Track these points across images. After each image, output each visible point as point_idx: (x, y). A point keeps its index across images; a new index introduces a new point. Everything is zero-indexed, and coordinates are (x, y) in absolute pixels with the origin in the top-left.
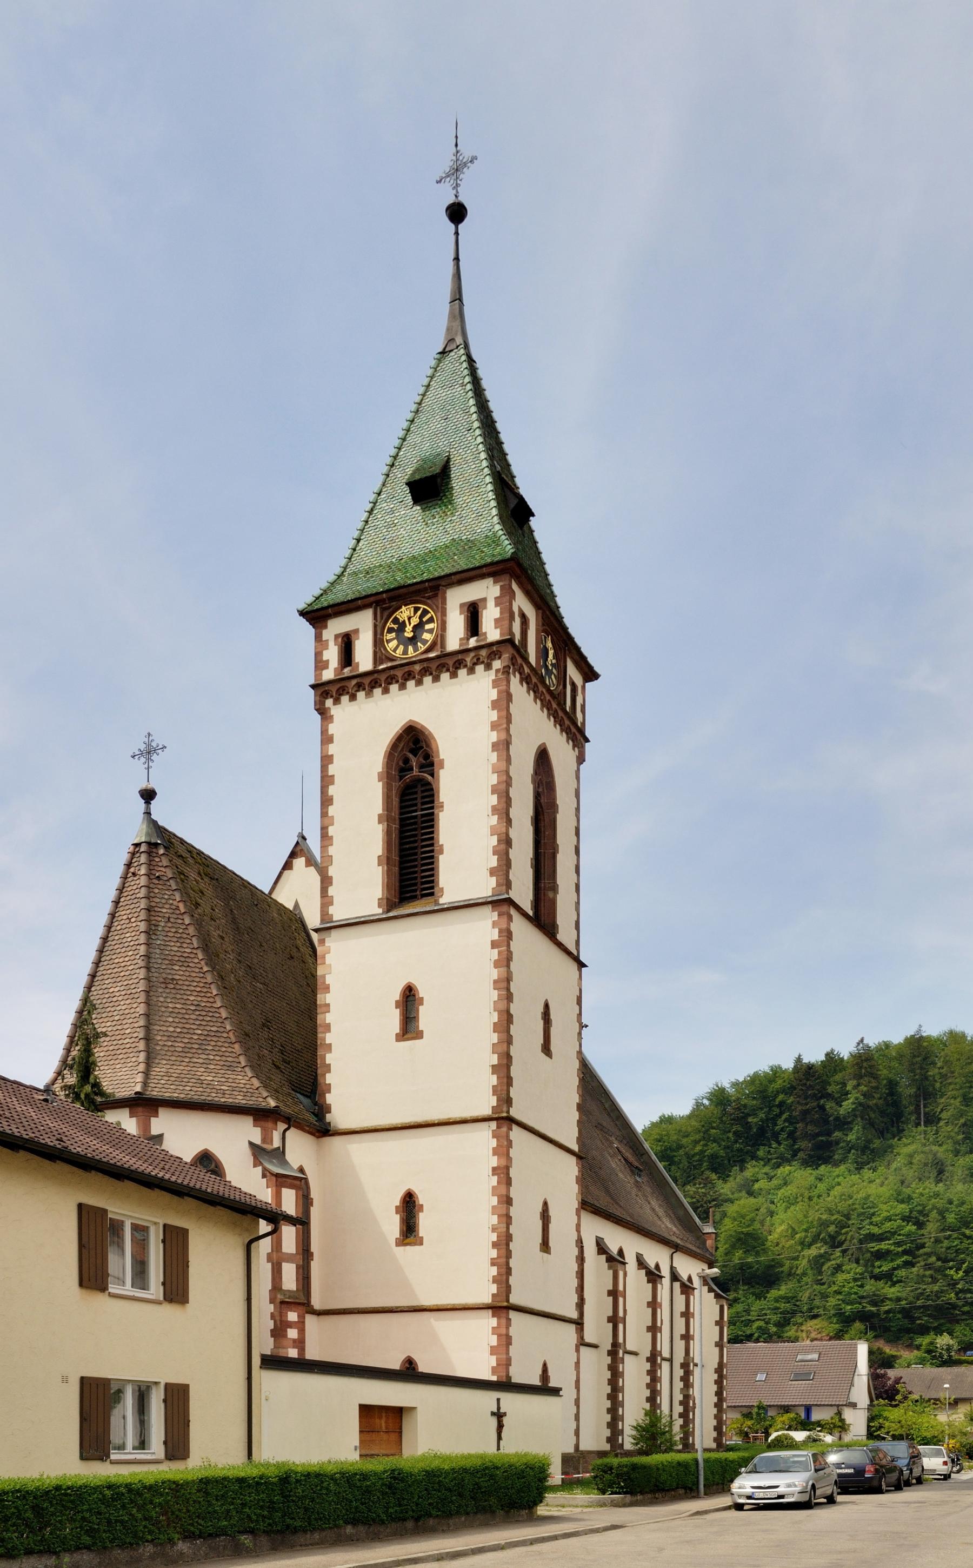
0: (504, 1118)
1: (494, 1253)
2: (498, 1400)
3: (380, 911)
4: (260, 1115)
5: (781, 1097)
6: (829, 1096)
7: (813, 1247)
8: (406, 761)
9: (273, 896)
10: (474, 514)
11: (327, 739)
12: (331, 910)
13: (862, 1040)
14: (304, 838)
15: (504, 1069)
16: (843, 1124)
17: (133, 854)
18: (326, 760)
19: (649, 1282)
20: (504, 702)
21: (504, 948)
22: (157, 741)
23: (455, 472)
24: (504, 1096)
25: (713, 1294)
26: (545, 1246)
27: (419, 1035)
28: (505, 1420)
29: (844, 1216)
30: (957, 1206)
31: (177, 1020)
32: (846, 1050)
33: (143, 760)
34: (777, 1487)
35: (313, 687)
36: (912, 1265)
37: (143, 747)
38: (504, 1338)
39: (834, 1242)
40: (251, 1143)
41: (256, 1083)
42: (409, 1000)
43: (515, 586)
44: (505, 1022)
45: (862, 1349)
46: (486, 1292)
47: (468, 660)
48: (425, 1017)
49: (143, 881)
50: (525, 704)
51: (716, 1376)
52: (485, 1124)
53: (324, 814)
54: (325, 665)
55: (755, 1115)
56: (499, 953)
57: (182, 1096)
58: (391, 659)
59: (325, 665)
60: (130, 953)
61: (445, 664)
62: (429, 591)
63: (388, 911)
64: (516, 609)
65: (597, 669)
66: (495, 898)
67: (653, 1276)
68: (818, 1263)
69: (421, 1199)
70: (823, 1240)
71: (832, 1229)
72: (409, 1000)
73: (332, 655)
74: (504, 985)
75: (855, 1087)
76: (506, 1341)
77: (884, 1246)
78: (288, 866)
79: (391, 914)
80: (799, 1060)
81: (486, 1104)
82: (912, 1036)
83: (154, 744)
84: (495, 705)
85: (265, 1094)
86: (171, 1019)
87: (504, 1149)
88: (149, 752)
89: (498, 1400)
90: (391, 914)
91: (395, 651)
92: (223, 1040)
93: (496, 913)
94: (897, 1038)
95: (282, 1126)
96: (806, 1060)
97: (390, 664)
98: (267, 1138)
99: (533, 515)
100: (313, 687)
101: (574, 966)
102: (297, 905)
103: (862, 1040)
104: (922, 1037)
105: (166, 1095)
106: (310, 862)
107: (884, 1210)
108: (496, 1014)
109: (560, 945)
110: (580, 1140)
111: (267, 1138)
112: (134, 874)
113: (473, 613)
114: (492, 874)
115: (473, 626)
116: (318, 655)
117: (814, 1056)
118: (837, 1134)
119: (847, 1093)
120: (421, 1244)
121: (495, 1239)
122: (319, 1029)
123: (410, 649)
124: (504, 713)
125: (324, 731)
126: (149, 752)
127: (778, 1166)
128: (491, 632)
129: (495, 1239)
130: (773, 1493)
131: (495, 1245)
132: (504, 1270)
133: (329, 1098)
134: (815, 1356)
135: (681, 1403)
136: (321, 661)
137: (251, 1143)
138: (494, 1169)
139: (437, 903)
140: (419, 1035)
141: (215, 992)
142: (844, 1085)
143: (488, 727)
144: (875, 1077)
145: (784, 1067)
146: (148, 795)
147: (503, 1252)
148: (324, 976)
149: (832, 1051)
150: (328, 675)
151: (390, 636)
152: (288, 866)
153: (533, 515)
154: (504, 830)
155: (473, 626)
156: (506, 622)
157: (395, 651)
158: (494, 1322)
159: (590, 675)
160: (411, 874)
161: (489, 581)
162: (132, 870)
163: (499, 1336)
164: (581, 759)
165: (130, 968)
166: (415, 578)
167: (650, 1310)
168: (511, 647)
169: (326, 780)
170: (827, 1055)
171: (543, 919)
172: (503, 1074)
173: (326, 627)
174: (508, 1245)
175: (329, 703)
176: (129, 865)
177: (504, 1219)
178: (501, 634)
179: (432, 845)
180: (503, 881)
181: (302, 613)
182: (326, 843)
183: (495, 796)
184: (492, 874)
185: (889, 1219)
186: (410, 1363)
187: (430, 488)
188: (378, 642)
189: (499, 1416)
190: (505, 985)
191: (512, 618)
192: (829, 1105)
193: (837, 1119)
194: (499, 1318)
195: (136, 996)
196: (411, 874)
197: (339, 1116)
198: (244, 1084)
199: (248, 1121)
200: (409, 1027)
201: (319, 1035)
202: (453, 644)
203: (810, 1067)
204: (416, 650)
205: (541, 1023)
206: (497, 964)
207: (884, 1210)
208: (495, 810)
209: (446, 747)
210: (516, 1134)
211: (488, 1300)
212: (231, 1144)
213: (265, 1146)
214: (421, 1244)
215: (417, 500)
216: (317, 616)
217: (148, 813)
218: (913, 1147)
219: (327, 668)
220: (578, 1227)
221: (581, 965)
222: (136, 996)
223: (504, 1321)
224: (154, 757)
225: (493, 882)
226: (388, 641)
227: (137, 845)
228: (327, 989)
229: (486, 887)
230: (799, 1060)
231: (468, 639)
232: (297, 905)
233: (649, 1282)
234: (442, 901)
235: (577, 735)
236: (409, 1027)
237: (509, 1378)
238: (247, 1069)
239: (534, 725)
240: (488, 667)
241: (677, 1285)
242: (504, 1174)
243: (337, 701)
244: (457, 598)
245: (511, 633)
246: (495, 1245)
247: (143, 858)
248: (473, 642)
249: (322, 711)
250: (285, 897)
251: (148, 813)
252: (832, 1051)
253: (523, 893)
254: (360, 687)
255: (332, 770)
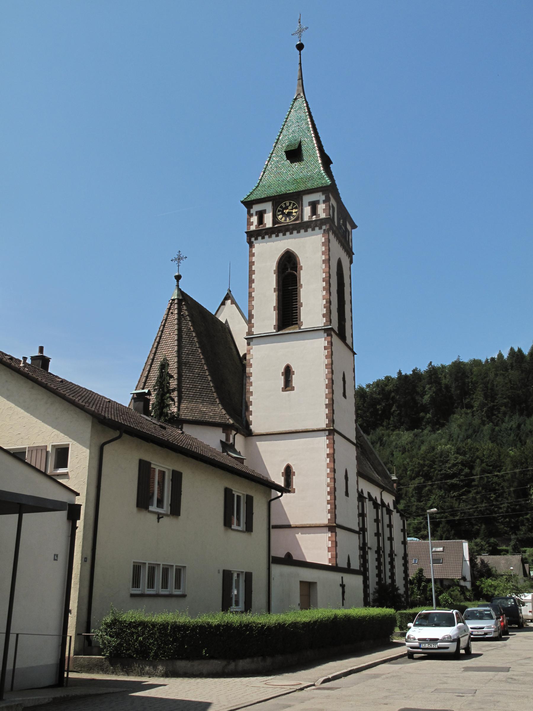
0: (331, 431)
1: (329, 498)
2: (342, 578)
3: (275, 331)
4: (226, 428)
5: (393, 394)
6: (418, 393)
7: (416, 479)
8: (285, 265)
9: (217, 316)
10: (311, 167)
11: (252, 255)
12: (253, 329)
13: (431, 362)
14: (230, 291)
15: (331, 405)
16: (425, 409)
17: (171, 304)
18: (252, 263)
19: (374, 508)
20: (327, 243)
21: (330, 350)
22: (183, 254)
23: (303, 148)
24: (331, 419)
25: (399, 514)
26: (347, 494)
27: (293, 389)
28: (346, 589)
29: (431, 461)
30: (487, 458)
31: (190, 381)
32: (423, 368)
33: (176, 262)
34: (483, 628)
35: (246, 232)
36: (469, 492)
37: (176, 257)
38: (334, 543)
39: (427, 477)
40: (221, 441)
41: (224, 412)
42: (288, 372)
43: (331, 196)
44: (331, 384)
45: (466, 545)
46: (324, 519)
47: (312, 225)
48: (295, 380)
49: (176, 316)
50: (335, 244)
51: (403, 562)
52: (323, 432)
53: (250, 287)
54: (252, 224)
55: (380, 404)
56: (328, 352)
57: (194, 418)
58: (281, 223)
59: (252, 224)
60: (170, 349)
61: (301, 227)
62: (296, 197)
63: (278, 331)
64: (331, 205)
65: (356, 223)
66: (326, 327)
67: (376, 505)
68: (419, 489)
69: (294, 469)
70: (422, 476)
71: (426, 468)
72: (288, 372)
73: (255, 219)
74: (330, 367)
75: (430, 389)
76: (335, 544)
77: (454, 481)
78: (223, 303)
79: (279, 333)
80: (400, 373)
81: (323, 423)
82: (456, 361)
83: (182, 256)
84: (323, 244)
85: (228, 417)
86: (188, 381)
87: (332, 445)
88: (179, 259)
89: (342, 578)
90: (279, 333)
91: (281, 219)
92: (209, 391)
93: (326, 334)
94: (448, 363)
95: (234, 432)
96: (403, 374)
97: (279, 225)
98: (228, 438)
99: (332, 163)
100: (246, 232)
101: (352, 354)
102: (226, 321)
103: (431, 362)
104: (460, 362)
105: (187, 418)
106: (233, 302)
107: (453, 458)
108: (327, 380)
109: (347, 345)
110: (357, 438)
111: (228, 438)
112: (172, 313)
113: (314, 205)
114: (324, 317)
115: (314, 211)
116: (249, 220)
117: (408, 371)
118: (422, 414)
119: (426, 392)
120: (294, 492)
121: (329, 490)
122: (247, 385)
123: (288, 219)
124: (328, 248)
125: (251, 251)
126: (179, 259)
127: (393, 430)
128: (322, 214)
129: (329, 490)
130: (481, 632)
131: (329, 493)
132: (333, 506)
133: (251, 418)
134: (441, 549)
135: (390, 577)
136: (250, 221)
137: (221, 441)
138: (328, 454)
139: (300, 329)
140: (293, 389)
141: (206, 368)
142: (424, 388)
143: (321, 253)
144: (440, 384)
145: (393, 376)
146: (178, 278)
147: (333, 496)
148: (249, 360)
149: (416, 368)
150: (253, 228)
151: (279, 213)
152: (223, 303)
153: (332, 163)
154: (328, 297)
155: (314, 211)
156: (328, 211)
157: (281, 219)
158: (329, 535)
159: (354, 226)
160: (288, 313)
161: (320, 194)
162: (171, 311)
163: (332, 542)
164: (351, 262)
165: (170, 356)
166: (290, 190)
167: (376, 524)
168: (328, 221)
169: (251, 272)
170: (414, 371)
171: (342, 334)
172: (331, 408)
173: (252, 208)
174: (335, 493)
175: (253, 239)
176: (169, 309)
177: (333, 480)
178: (326, 215)
179: (297, 302)
180: (329, 320)
181: (242, 202)
182: (251, 299)
183: (324, 283)
184: (324, 317)
185: (454, 465)
186: (289, 555)
187: (294, 154)
188: (275, 216)
189: (343, 586)
190: (331, 366)
191: (330, 209)
192: (418, 398)
193: (422, 405)
194: (332, 532)
195: (173, 370)
196: (288, 313)
197: (255, 428)
198: (218, 412)
199: (220, 430)
200: (288, 385)
201: (247, 387)
202: (306, 219)
203: (406, 376)
204: (290, 219)
205: (342, 382)
206: (327, 357)
207: (453, 458)
208: (324, 289)
209: (303, 261)
210: (337, 437)
211: (326, 522)
212: (210, 439)
213: (227, 442)
214: (294, 492)
215: (288, 158)
216: (248, 204)
217: (178, 286)
218: (458, 421)
219: (252, 225)
220: (357, 481)
221: (354, 354)
222: (173, 370)
223: (334, 534)
224: (181, 261)
225: (324, 320)
226: (278, 215)
227: (173, 300)
228: (251, 365)
229: (321, 322)
230: (400, 373)
231: (312, 216)
232: (226, 321)
233: (374, 508)
234: (302, 328)
235: (350, 253)
236: (288, 385)
237: (337, 564)
238: (220, 405)
239: (338, 251)
240: (320, 228)
241: (384, 509)
242: (332, 456)
243: (256, 239)
244: (307, 199)
245: (330, 215)
246: (329, 493)
247: (176, 306)
248: (314, 218)
249: (251, 244)
250: (222, 318)
251: (178, 286)
252: (416, 368)
253: (335, 325)
254: (266, 234)
255: (254, 268)
